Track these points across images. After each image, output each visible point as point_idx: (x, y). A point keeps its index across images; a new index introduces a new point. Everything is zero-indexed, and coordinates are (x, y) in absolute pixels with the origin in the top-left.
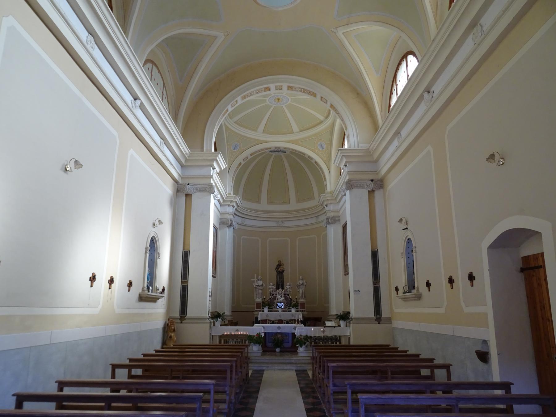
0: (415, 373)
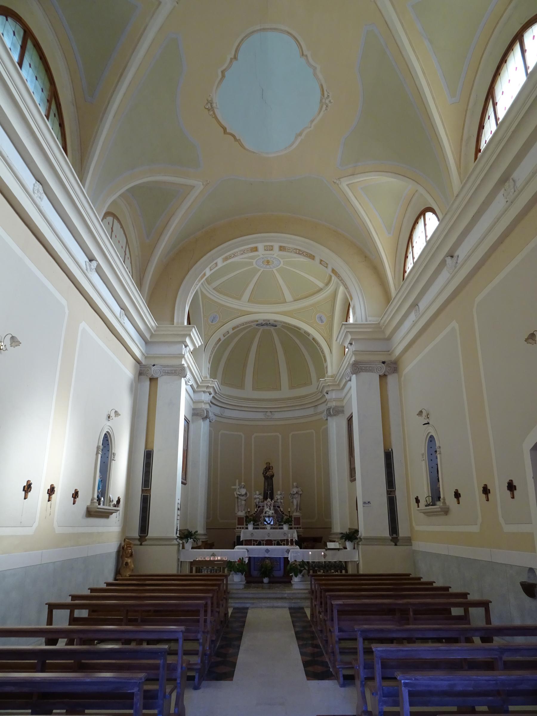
0: (443, 612)
